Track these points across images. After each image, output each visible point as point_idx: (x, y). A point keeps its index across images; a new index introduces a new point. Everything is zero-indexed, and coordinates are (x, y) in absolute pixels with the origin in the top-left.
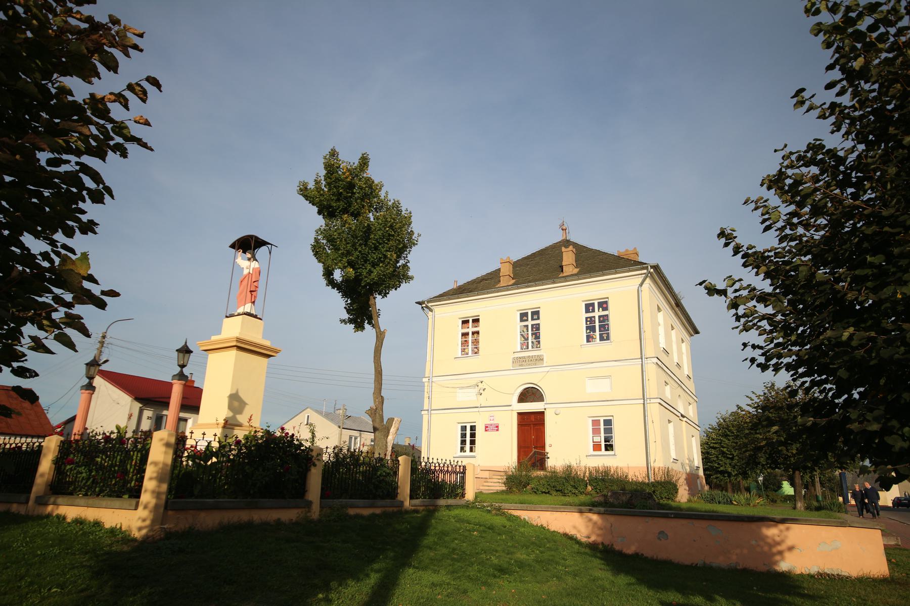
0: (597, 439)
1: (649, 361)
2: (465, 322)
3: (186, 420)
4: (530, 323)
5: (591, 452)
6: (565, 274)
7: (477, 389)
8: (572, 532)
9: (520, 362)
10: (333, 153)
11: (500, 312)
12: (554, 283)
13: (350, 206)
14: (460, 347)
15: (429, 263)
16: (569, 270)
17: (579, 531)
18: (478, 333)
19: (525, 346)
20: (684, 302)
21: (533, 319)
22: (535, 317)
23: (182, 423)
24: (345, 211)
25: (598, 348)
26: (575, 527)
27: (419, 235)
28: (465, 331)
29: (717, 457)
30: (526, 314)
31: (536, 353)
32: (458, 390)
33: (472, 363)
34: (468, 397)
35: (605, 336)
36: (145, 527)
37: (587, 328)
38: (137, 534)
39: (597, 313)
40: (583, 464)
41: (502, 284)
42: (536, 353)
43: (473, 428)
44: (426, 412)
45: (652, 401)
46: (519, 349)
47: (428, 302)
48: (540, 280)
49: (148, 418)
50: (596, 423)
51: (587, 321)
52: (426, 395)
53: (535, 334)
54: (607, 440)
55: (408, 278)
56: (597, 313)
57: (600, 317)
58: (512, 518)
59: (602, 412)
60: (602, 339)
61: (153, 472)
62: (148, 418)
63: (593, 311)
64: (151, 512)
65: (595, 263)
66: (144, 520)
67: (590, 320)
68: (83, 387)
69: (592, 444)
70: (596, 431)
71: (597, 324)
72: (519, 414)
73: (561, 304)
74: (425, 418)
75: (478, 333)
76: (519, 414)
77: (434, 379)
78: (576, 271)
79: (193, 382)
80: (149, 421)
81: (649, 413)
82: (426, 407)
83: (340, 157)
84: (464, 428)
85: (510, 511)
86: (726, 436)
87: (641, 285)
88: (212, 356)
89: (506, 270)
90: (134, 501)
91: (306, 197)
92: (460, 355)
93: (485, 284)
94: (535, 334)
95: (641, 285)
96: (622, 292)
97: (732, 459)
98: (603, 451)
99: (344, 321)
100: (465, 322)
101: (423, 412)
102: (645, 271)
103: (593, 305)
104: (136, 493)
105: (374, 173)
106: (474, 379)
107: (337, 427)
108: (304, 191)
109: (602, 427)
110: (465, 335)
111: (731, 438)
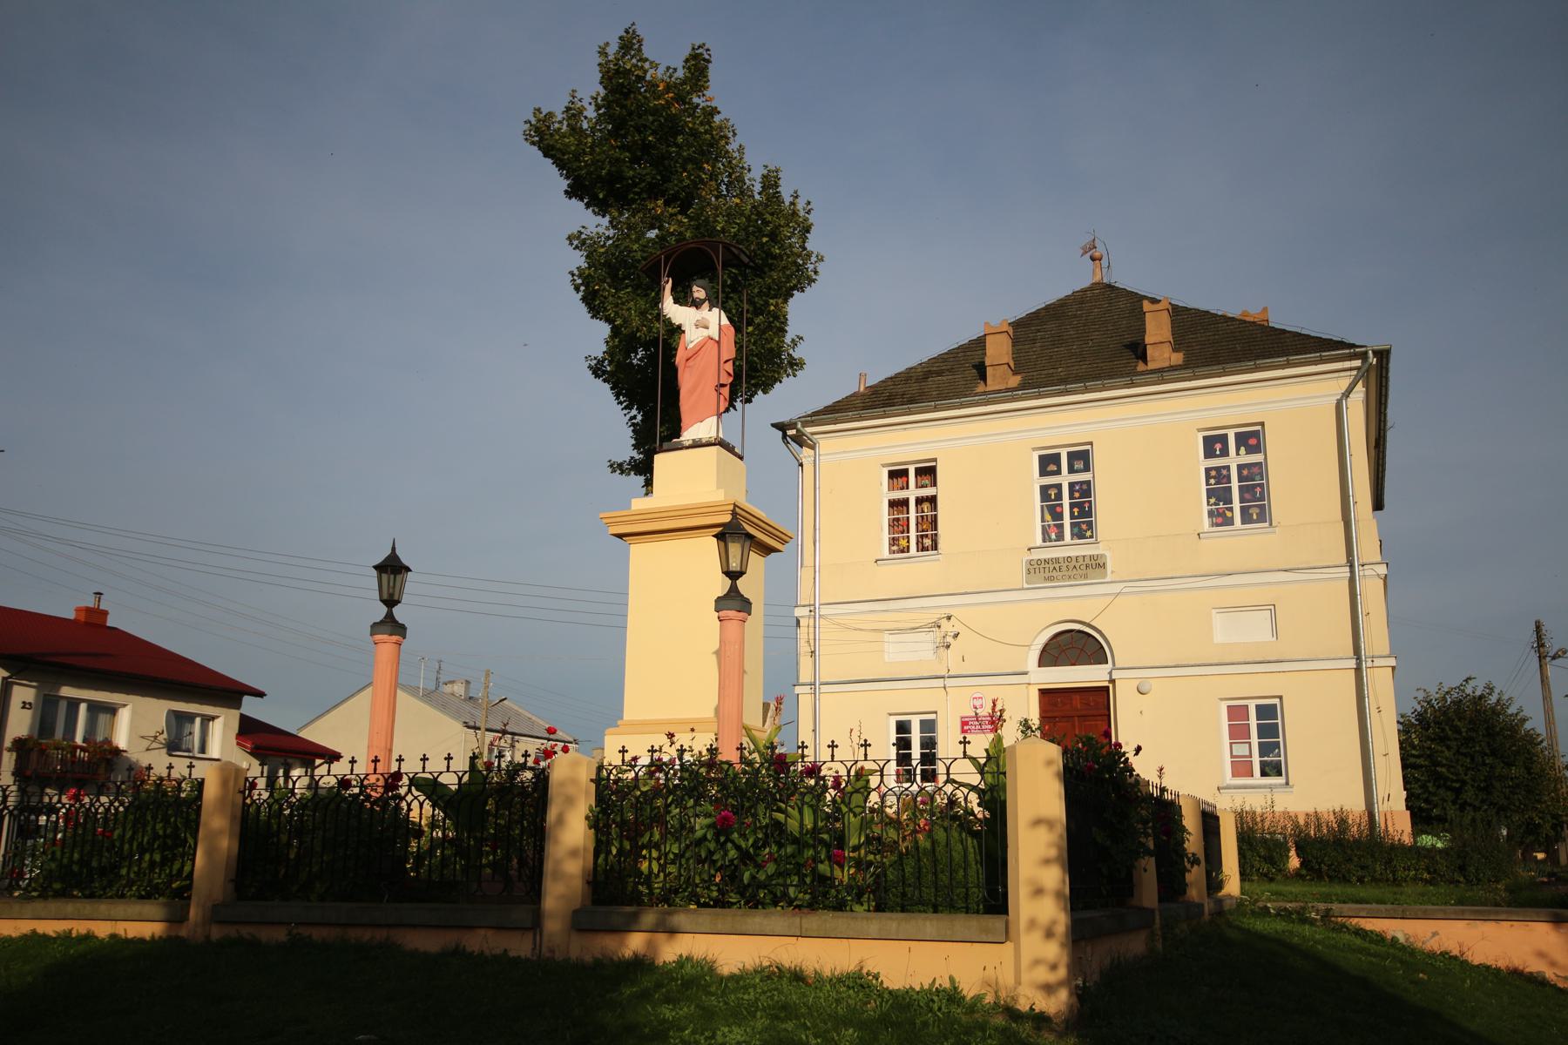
0: (1241, 750)
1: (1368, 571)
2: (897, 475)
3: (112, 710)
4: (1065, 479)
5: (1229, 779)
6: (1151, 366)
7: (938, 634)
8: (1535, 966)
9: (1044, 571)
10: (629, 43)
11: (989, 453)
12: (1132, 385)
13: (666, 180)
14: (886, 537)
15: (839, 327)
16: (1161, 354)
17: (1553, 964)
18: (932, 500)
19: (1052, 533)
20: (1391, 436)
21: (1071, 470)
22: (1079, 465)
23: (103, 718)
24: (654, 191)
25: (1242, 541)
26: (1541, 955)
27: (821, 259)
28: (899, 495)
29: (1423, 787)
30: (1056, 459)
31: (1082, 550)
32: (886, 637)
33: (918, 570)
34: (916, 652)
35: (1254, 512)
36: (1060, 984)
37: (1210, 493)
38: (1056, 1004)
39: (1234, 460)
40: (1278, 809)
41: (992, 384)
42: (1082, 550)
43: (928, 726)
44: (807, 689)
45: (1378, 662)
46: (1039, 541)
47: (805, 424)
48: (1078, 379)
49: (25, 705)
50: (1237, 712)
51: (1208, 477)
52: (804, 648)
53: (1080, 505)
54: (1265, 750)
55: (795, 365)
56: (1234, 460)
57: (1240, 467)
58: (1360, 933)
59: (1255, 687)
60: (1246, 518)
61: (1049, 845)
62: (25, 705)
63: (1225, 453)
64: (1063, 945)
65: (1225, 344)
66: (1054, 967)
67: (1217, 477)
68: (376, 628)
69: (1228, 760)
70: (1238, 733)
71: (1235, 485)
72: (1043, 692)
73: (1145, 436)
74: (805, 702)
75: (932, 500)
76: (1043, 692)
77: (825, 611)
78: (1177, 358)
79: (105, 613)
80: (28, 714)
81: (1369, 691)
82: (805, 675)
83: (647, 52)
84: (903, 727)
85: (1355, 921)
86: (1442, 739)
87: (1347, 394)
88: (639, 552)
89: (999, 352)
90: (996, 922)
91: (548, 151)
92: (886, 554)
93: (949, 380)
94: (1080, 505)
95: (1347, 394)
96: (1301, 411)
97: (1458, 792)
98: (1257, 778)
99: (620, 465)
100: (897, 475)
101: (798, 690)
102: (1357, 363)
103: (1223, 439)
104: (995, 901)
105: (724, 94)
106: (933, 609)
107: (459, 726)
108: (544, 137)
109: (1253, 722)
110: (898, 505)
111: (1453, 744)
